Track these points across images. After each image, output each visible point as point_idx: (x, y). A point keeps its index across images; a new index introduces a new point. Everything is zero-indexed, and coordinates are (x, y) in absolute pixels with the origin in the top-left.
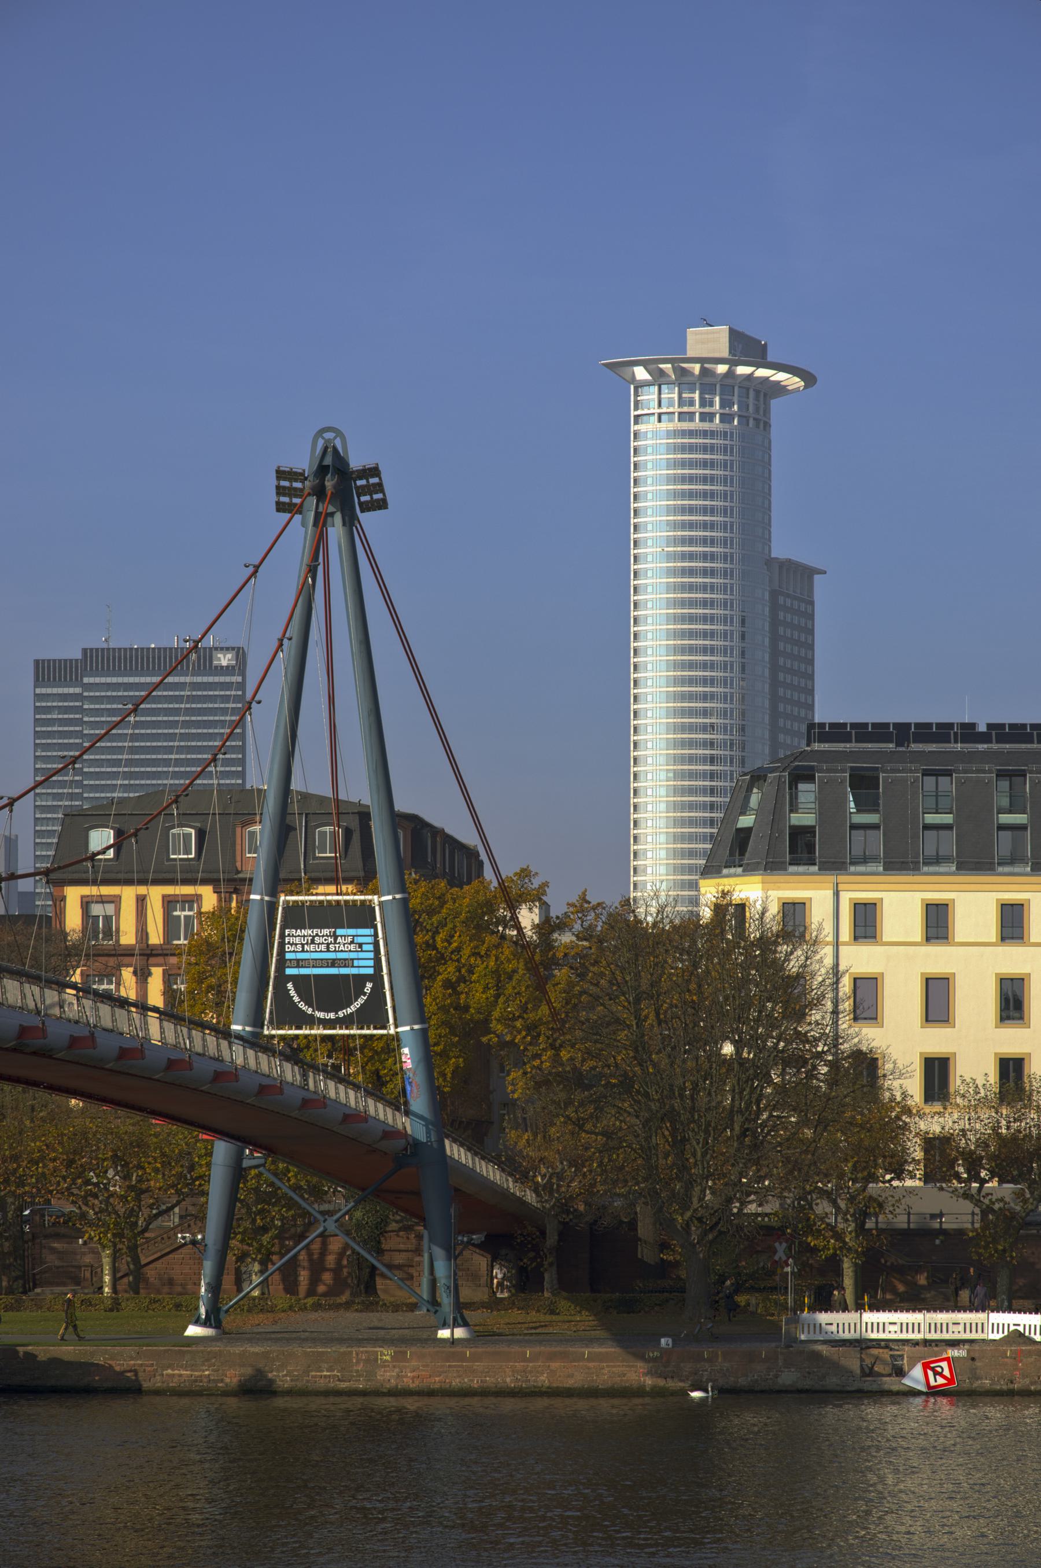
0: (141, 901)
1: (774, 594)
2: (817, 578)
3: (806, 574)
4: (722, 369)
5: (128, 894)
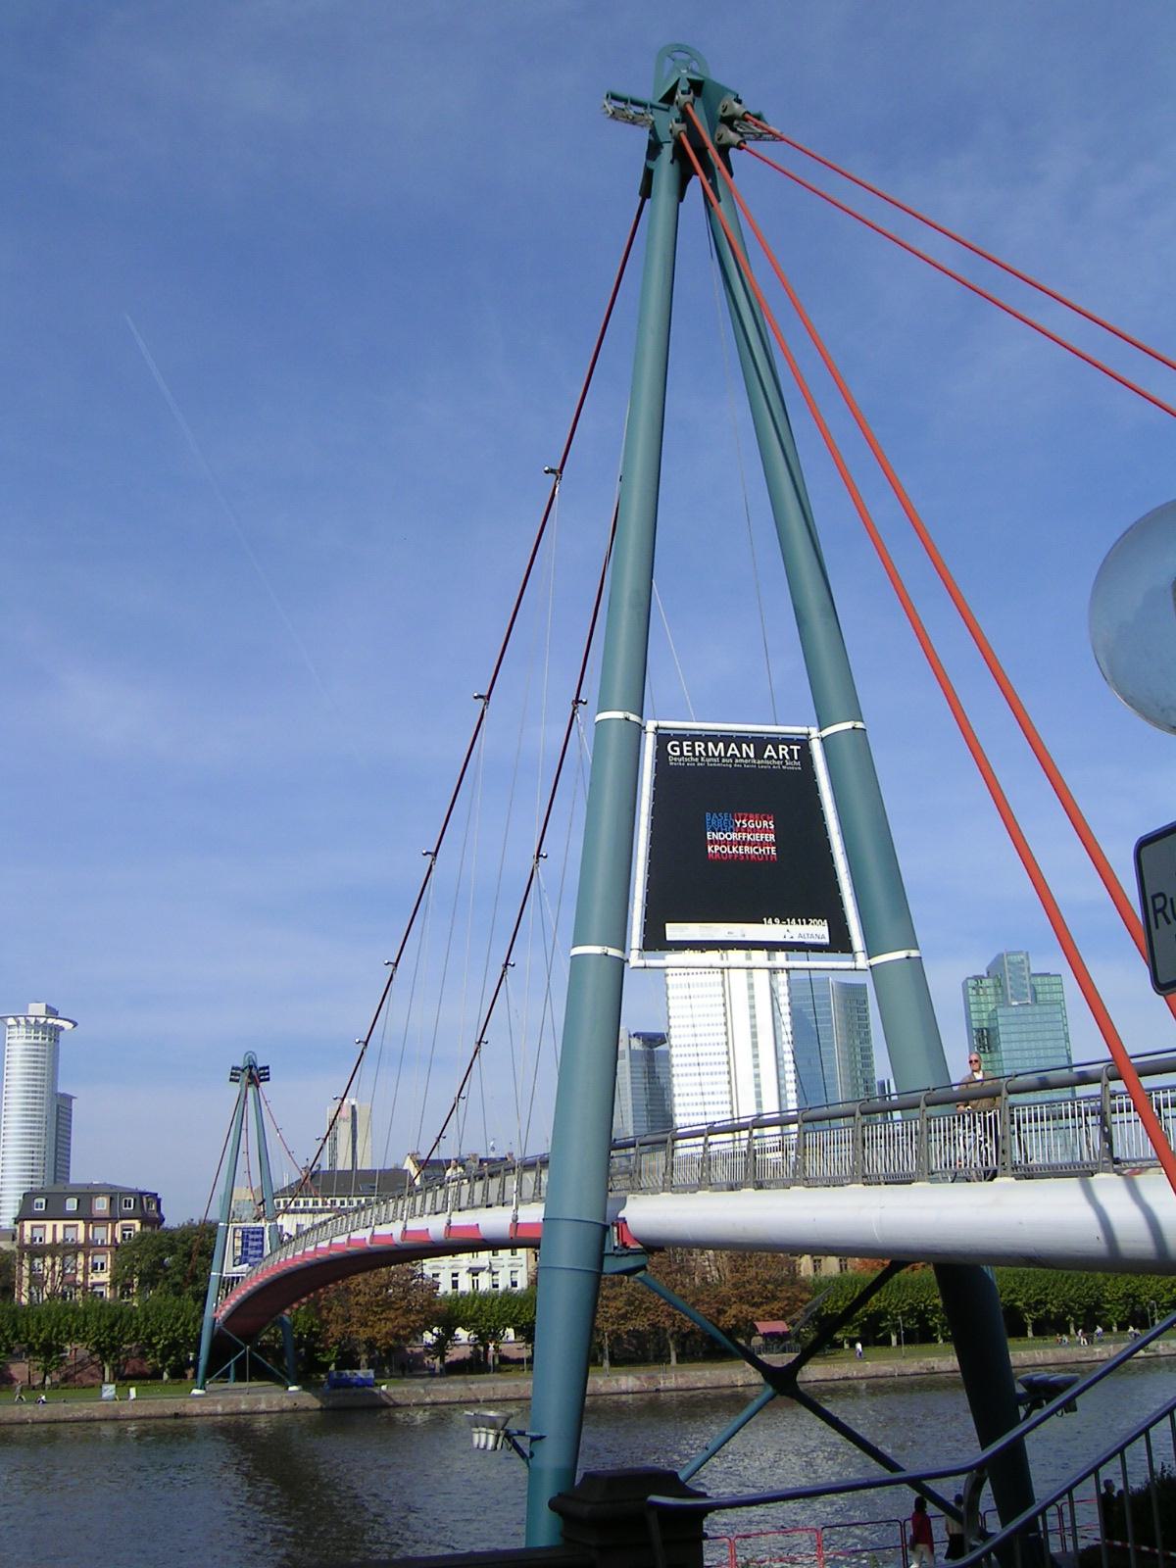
0: (55, 1226)
1: (58, 1106)
2: (73, 1100)
3: (69, 1099)
4: (42, 1020)
5: (49, 1224)
